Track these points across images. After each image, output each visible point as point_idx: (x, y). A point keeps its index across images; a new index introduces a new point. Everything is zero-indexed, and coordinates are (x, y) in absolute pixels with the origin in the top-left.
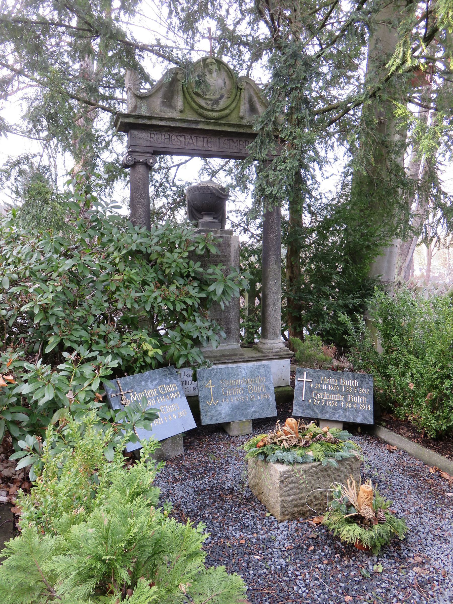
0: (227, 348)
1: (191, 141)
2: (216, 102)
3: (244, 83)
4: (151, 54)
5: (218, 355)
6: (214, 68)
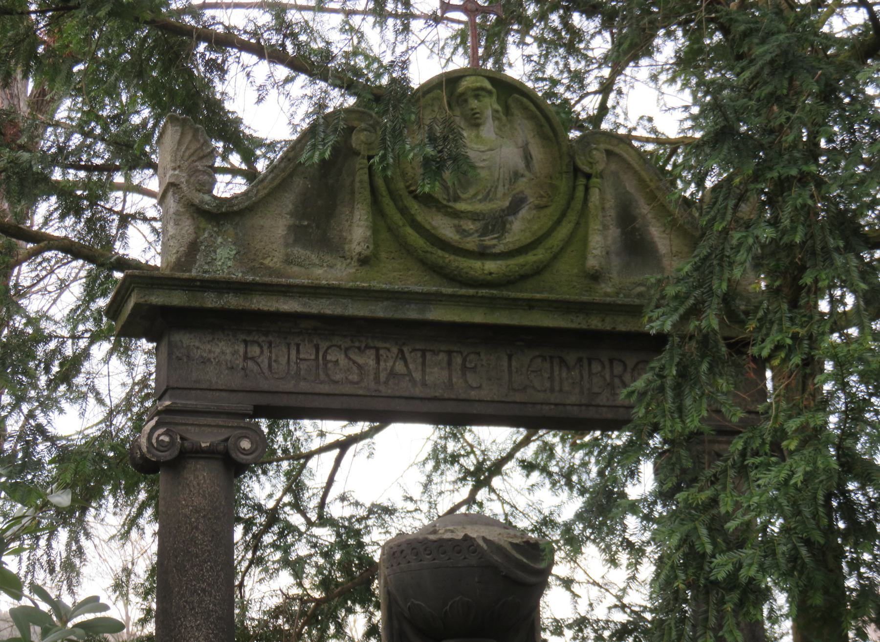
1: (400, 367)
2: (497, 223)
3: (598, 155)
4: (248, 58)
6: (489, 106)
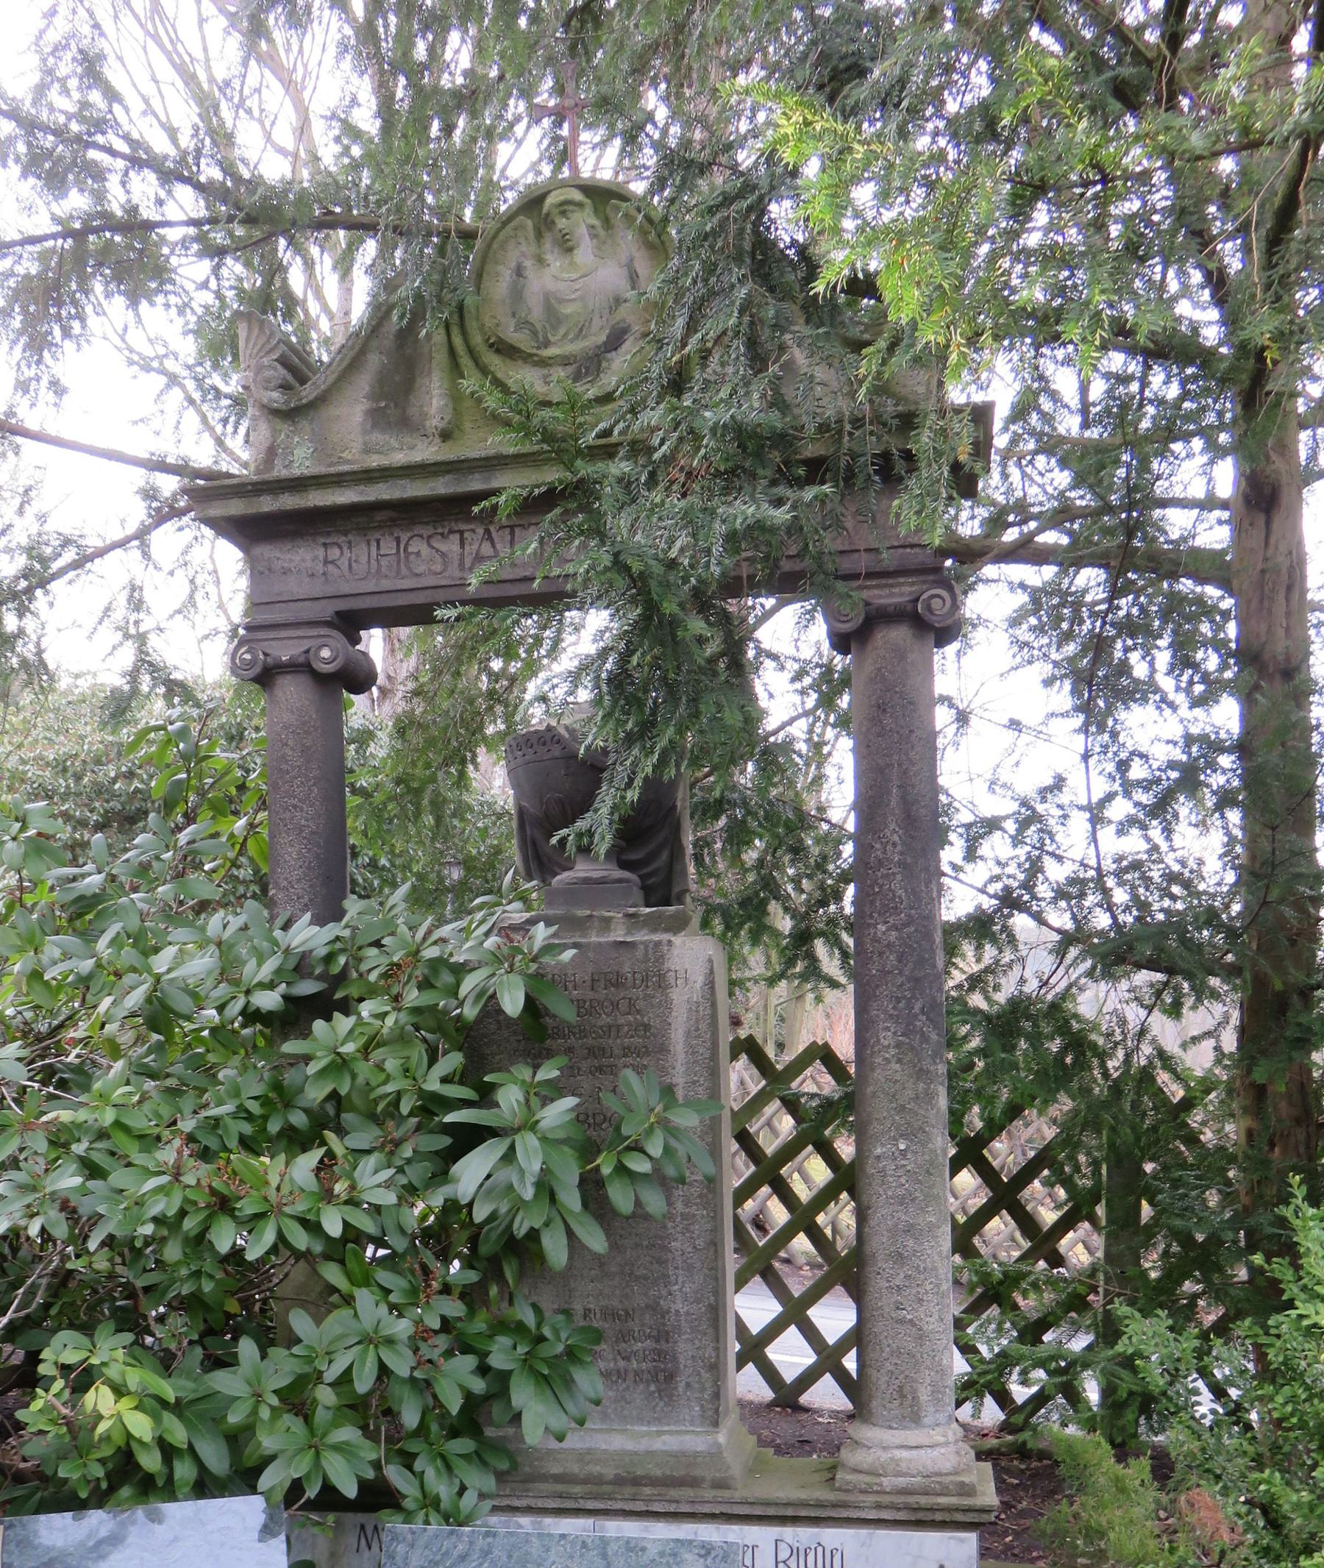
0: (658, 1444)
1: (486, 549)
5: (609, 1472)
6: (582, 222)
